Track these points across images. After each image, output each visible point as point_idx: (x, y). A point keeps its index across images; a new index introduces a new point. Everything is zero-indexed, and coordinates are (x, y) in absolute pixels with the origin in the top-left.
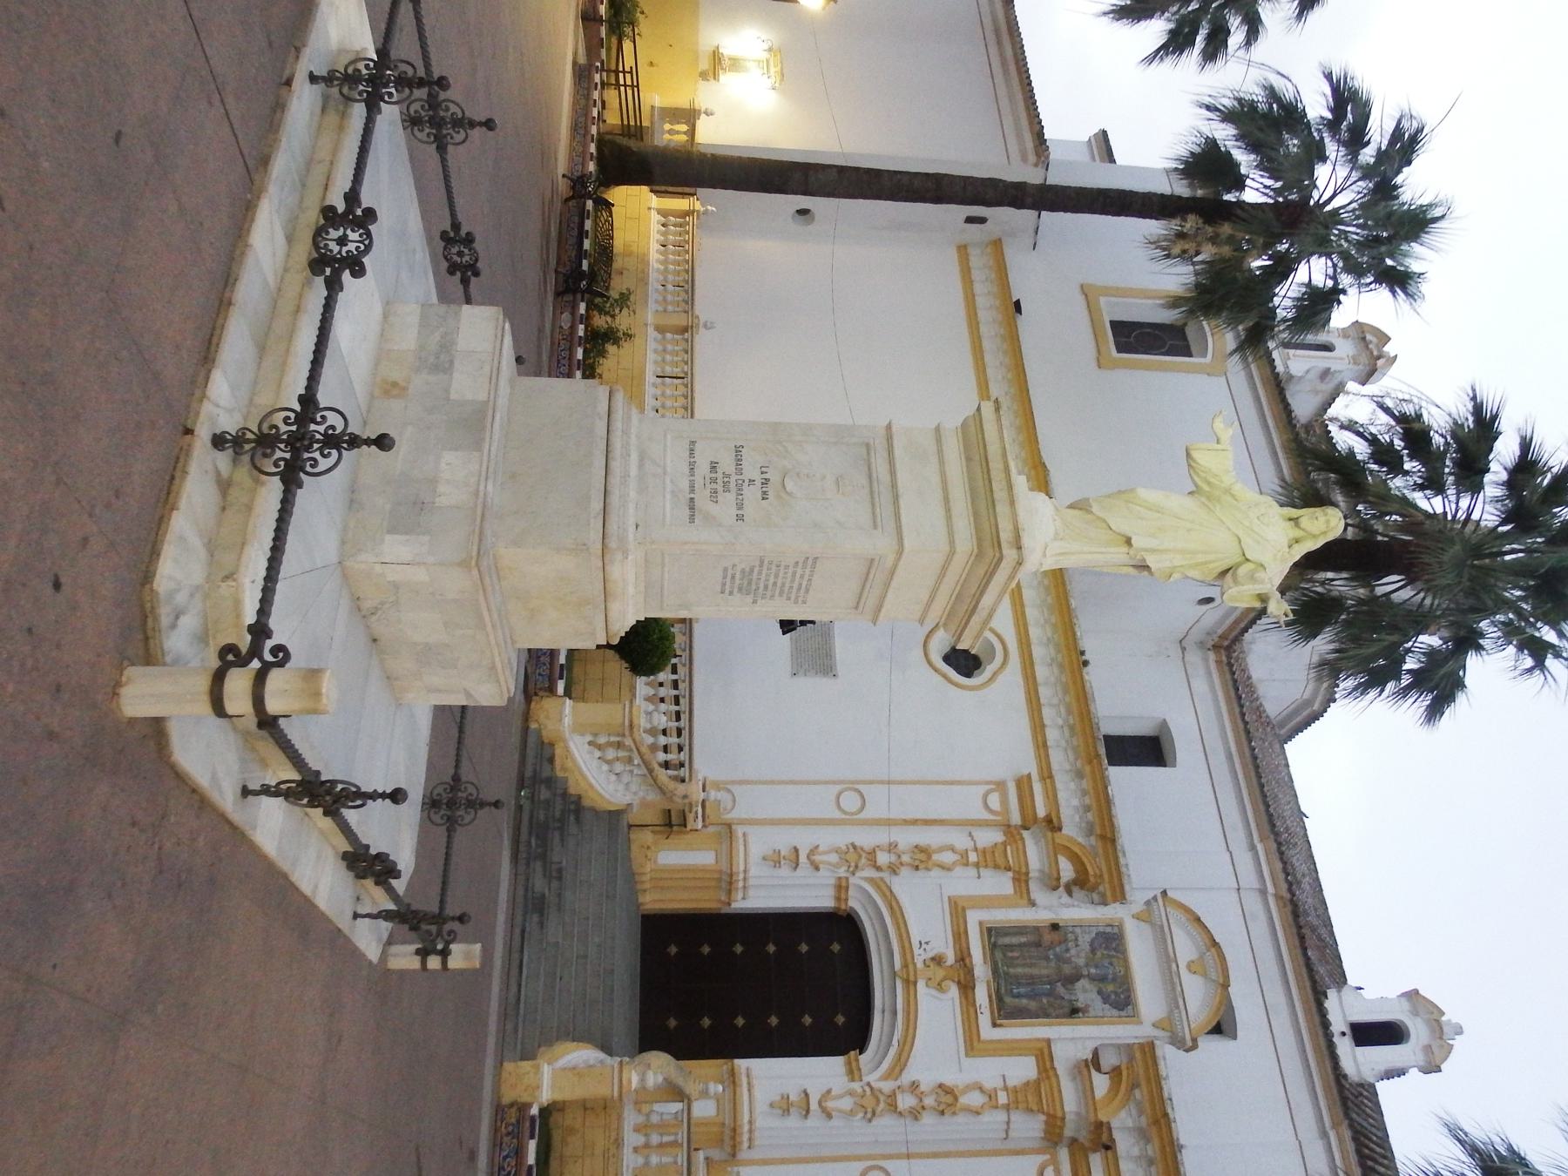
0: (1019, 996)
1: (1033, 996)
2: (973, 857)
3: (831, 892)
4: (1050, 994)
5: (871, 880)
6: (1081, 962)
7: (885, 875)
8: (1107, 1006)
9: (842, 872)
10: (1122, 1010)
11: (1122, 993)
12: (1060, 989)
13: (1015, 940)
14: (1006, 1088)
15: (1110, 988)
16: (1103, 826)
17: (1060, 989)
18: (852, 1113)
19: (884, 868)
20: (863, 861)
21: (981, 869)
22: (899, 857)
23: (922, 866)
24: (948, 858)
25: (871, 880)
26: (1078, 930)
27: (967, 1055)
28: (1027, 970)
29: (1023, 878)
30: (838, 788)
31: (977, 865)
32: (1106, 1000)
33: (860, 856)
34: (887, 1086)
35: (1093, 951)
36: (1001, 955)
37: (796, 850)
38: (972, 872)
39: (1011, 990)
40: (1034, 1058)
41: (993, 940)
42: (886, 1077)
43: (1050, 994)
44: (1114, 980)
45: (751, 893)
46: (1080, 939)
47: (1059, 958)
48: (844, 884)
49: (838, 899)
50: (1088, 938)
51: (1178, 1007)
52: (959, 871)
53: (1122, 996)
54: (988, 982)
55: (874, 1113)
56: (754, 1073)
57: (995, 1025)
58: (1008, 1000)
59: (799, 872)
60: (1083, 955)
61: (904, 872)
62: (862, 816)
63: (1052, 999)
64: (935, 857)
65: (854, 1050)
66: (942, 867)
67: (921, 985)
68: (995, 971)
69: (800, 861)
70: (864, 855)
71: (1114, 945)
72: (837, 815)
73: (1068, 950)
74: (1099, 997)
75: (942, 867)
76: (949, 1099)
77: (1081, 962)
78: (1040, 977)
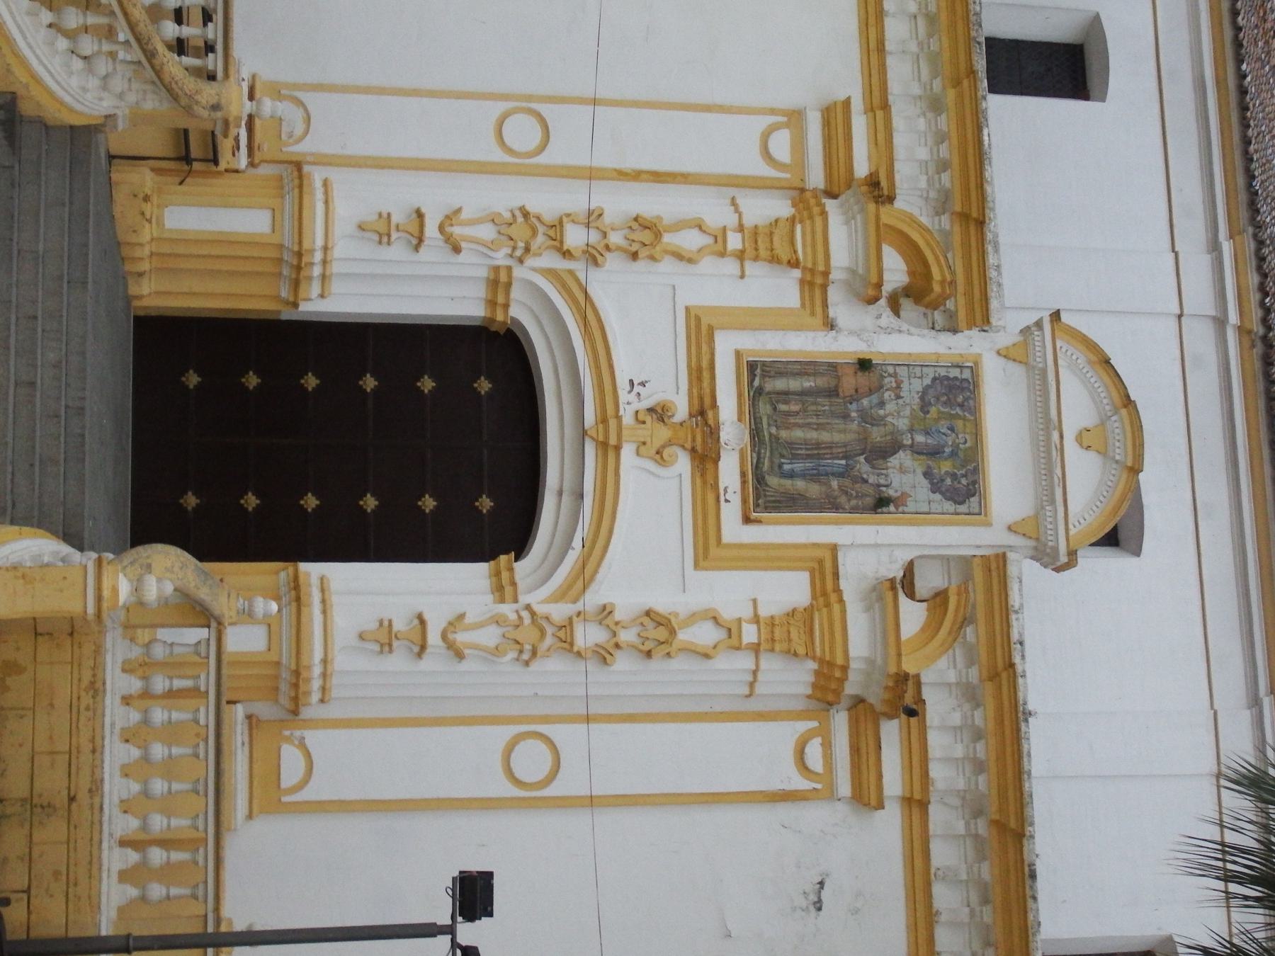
0: (791, 475)
1: (814, 476)
3: (481, 291)
5: (551, 274)
6: (903, 424)
7: (578, 267)
8: (938, 496)
9: (501, 258)
12: (862, 466)
18: (497, 651)
24: (691, 240)
25: (551, 274)
27: (697, 566)
30: (502, 106)
31: (741, 256)
32: (935, 488)
34: (559, 612)
35: (925, 406)
38: (731, 266)
39: (780, 466)
41: (756, 383)
42: (561, 596)
44: (954, 454)
45: (336, 287)
46: (905, 386)
48: (503, 277)
49: (492, 303)
50: (917, 385)
52: (708, 264)
58: (773, 481)
60: (907, 412)
61: (613, 262)
62: (542, 159)
63: (847, 482)
67: (627, 452)
68: (756, 434)
71: (960, 399)
72: (498, 156)
73: (882, 404)
77: (903, 424)
78: (831, 446)
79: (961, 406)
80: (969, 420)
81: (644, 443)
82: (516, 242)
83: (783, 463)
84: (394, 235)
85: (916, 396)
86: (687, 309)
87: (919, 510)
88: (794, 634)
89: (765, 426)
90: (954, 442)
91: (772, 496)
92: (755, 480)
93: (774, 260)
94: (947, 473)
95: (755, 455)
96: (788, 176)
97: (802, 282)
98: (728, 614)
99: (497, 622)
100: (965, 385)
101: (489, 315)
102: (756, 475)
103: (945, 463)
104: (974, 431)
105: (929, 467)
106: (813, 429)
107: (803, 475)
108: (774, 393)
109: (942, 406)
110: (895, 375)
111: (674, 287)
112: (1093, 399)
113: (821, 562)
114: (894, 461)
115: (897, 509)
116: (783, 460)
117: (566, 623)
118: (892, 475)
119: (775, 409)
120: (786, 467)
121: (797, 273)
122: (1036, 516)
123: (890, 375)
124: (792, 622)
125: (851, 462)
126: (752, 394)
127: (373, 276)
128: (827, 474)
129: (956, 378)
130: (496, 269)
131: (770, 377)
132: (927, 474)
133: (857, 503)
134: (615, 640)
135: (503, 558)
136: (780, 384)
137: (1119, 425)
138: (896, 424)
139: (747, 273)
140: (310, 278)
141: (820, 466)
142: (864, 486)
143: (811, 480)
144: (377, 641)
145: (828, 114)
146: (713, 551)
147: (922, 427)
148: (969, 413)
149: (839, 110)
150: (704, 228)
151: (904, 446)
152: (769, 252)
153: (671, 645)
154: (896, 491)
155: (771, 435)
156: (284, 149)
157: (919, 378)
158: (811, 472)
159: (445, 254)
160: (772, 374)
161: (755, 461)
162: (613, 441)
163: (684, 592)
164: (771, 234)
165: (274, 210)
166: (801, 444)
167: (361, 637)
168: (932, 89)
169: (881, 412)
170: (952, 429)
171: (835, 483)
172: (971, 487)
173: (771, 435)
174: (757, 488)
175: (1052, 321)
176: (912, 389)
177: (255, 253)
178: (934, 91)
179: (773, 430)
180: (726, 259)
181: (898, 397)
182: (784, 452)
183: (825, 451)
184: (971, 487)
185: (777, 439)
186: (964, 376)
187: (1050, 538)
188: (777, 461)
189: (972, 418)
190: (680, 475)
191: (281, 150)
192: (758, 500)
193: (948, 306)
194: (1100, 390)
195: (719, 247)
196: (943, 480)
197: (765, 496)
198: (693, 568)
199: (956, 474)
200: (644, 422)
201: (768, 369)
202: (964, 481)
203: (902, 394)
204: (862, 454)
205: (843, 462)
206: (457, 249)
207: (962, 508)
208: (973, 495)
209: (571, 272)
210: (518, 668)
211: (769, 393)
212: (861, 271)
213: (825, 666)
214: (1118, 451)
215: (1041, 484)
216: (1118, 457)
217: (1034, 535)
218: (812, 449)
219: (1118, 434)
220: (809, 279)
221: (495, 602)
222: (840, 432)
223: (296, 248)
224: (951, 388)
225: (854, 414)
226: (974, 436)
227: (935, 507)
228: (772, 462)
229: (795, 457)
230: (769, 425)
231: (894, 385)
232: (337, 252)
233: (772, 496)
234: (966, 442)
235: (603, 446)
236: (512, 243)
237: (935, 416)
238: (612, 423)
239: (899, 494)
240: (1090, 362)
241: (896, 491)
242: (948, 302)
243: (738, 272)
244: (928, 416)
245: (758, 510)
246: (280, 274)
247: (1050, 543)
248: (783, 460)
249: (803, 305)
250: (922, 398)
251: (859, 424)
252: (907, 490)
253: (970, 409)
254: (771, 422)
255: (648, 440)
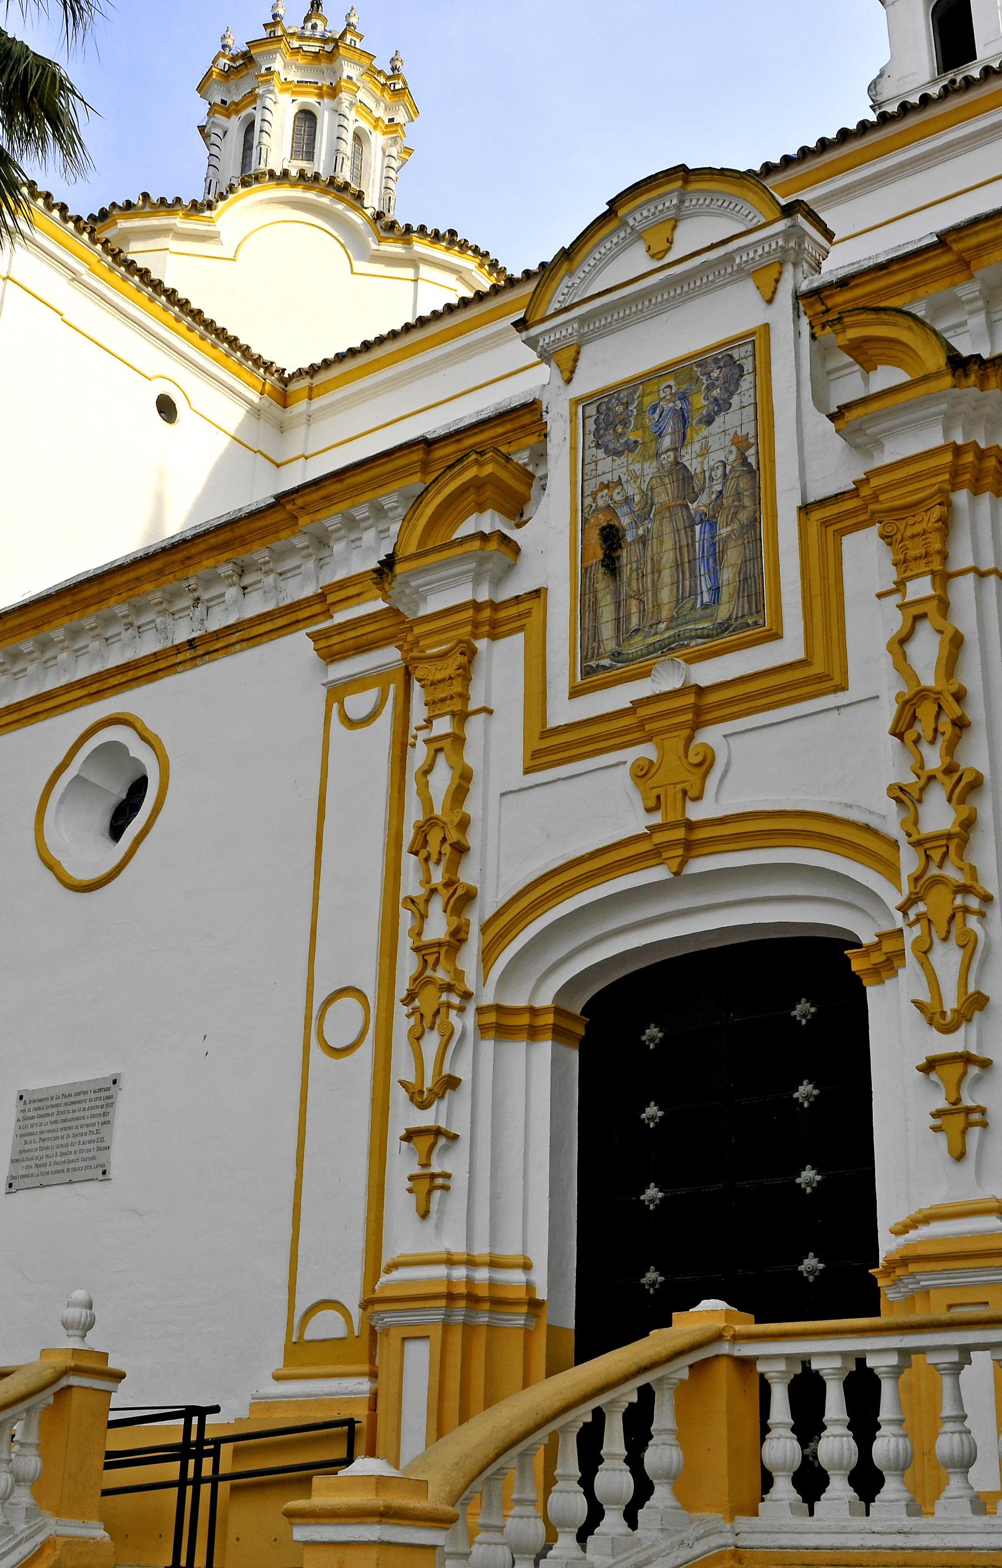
0: (716, 591)
1: (716, 555)
2: (921, 588)
3: (517, 1050)
4: (710, 521)
5: (488, 955)
6: (650, 468)
7: (476, 917)
8: (735, 400)
9: (465, 1022)
10: (741, 367)
11: (708, 375)
12: (701, 504)
13: (607, 613)
14: (900, 586)
15: (699, 401)
16: (403, 472)
17: (701, 504)
18: (969, 945)
19: (964, 812)
20: (951, 873)
21: (954, 566)
22: (932, 778)
23: (952, 709)
24: (441, 780)
25: (488, 955)
26: (591, 486)
27: (843, 687)
28: (667, 576)
29: (486, 613)
30: (316, 1050)
31: (461, 717)
32: (722, 406)
33: (938, 881)
34: (909, 861)
35: (631, 447)
36: (637, 639)
37: (930, 1066)
38: (474, 726)
39: (705, 606)
40: (843, 538)
41: (606, 662)
42: (890, 870)
43: (710, 521)
44: (684, 397)
45: (511, 1249)
46: (605, 479)
47: (643, 516)
48: (491, 1018)
49: (533, 1033)
50: (606, 463)
51: (729, 258)
52: (472, 757)
53: (715, 374)
54: (690, 661)
55: (965, 890)
56: (902, 1216)
57: (775, 636)
58: (723, 612)
59: (460, 1127)
60: (637, 467)
61: (468, 875)
62: (371, 992)
63: (721, 519)
64: (928, 679)
65: (847, 961)
66: (460, 792)
67: (696, 812)
68: (665, 648)
69: (960, 1049)
70: (934, 871)
71: (620, 409)
72: (366, 1051)
73: (628, 500)
74: (719, 420)
75: (460, 792)
76: (926, 711)
77: (650, 468)
78: (678, 548)
79: (627, 405)
80: (643, 390)
81: (685, 793)
82: (441, 1004)
83: (702, 604)
84: (435, 1169)
85: (618, 461)
86: (527, 771)
87: (752, 418)
88: (918, 529)
89: (657, 638)
90: (669, 401)
91: (743, 607)
92: (724, 635)
93: (465, 673)
94: (706, 398)
95: (693, 643)
96: (392, 687)
97: (494, 637)
98: (896, 622)
99: (925, 953)
100: (604, 407)
101: (550, 1035)
102: (718, 635)
103: (694, 402)
104: (656, 380)
105: (700, 421)
106: (659, 577)
107: (715, 574)
108: (618, 637)
109: (628, 428)
110: (594, 495)
111: (502, 795)
112: (614, 257)
113: (825, 523)
114: (693, 465)
115: (753, 444)
116: (698, 606)
117: (921, 850)
118: (712, 463)
119: (637, 631)
120: (706, 599)
121: (481, 644)
122: (754, 273)
123: (594, 500)
124: (899, 536)
125: (698, 519)
126: (619, 665)
127: (495, 1197)
128: (714, 544)
129: (596, 421)
130: (482, 1029)
131: (599, 647)
132: (709, 421)
133: (748, 496)
134: (940, 776)
135: (856, 966)
136: (607, 631)
137: (637, 215)
138: (650, 476)
139: (482, 705)
140: (492, 1284)
141: (703, 557)
142: (725, 495)
143: (721, 564)
144: (964, 1132)
145: (330, 656)
146: (817, 668)
147: (653, 443)
148: (635, 392)
149: (323, 644)
150: (426, 768)
151: (676, 458)
152: (454, 682)
153: (940, 693)
154: (731, 452)
155: (667, 629)
156: (356, 1334)
157: (596, 465)
158: (711, 565)
159: (461, 1101)
160: (595, 644)
161: (700, 641)
162: (680, 834)
163: (877, 697)
164: (432, 684)
165: (404, 1339)
166: (678, 587)
167: (960, 1156)
168: (307, 547)
169: (637, 498)
170: (654, 408)
171: (724, 531)
172: (722, 364)
173: (667, 629)
174: (733, 631)
175: (527, 328)
176: (608, 467)
177: (455, 1360)
178: (307, 543)
179: (662, 626)
180: (468, 735)
181: (619, 482)
182: (688, 606)
183: (686, 555)
184: (722, 364)
185: (672, 619)
186: (594, 412)
187: (774, 246)
188: (699, 613)
189: (641, 387)
190: (725, 736)
191: (357, 1337)
192: (748, 625)
193: (526, 460)
194: (603, 251)
195: (446, 744)
196: (716, 400)
197: (743, 616)
198: (846, 692)
199: (707, 388)
200: (658, 797)
201: (590, 651)
202: (715, 374)
203: (616, 479)
204: (687, 507)
205: (698, 528)
206: (452, 1083)
207: (748, 366)
208: (731, 356)
209: (484, 929)
210: (995, 913)
211: (619, 645)
212: (473, 565)
213: (961, 479)
214: (667, 204)
215: (713, 281)
216: (675, 201)
217: (777, 268)
218: (683, 573)
219: (649, 210)
220: (486, 628)
221: (904, 966)
222: (661, 543)
223: (443, 1303)
224: (610, 425)
225: (641, 532)
226: (662, 379)
227: (748, 400)
228: (702, 619)
229: (693, 592)
230: (656, 633)
231: (606, 491)
232: (458, 1247)
233: (743, 607)
234: (670, 387)
235: (690, 848)
236: (443, 1010)
237: (640, 432)
238: (658, 838)
239: (734, 448)
240: (570, 273)
241: (731, 452)
242: (521, 462)
243: (482, 716)
244: (640, 441)
245: (761, 621)
246: (489, 1326)
247: (781, 243)
248: (698, 606)
249: (521, 628)
250: (617, 453)
251: (652, 521)
252: (728, 438)
253: (631, 393)
254: (653, 631)
255: (679, 787)
